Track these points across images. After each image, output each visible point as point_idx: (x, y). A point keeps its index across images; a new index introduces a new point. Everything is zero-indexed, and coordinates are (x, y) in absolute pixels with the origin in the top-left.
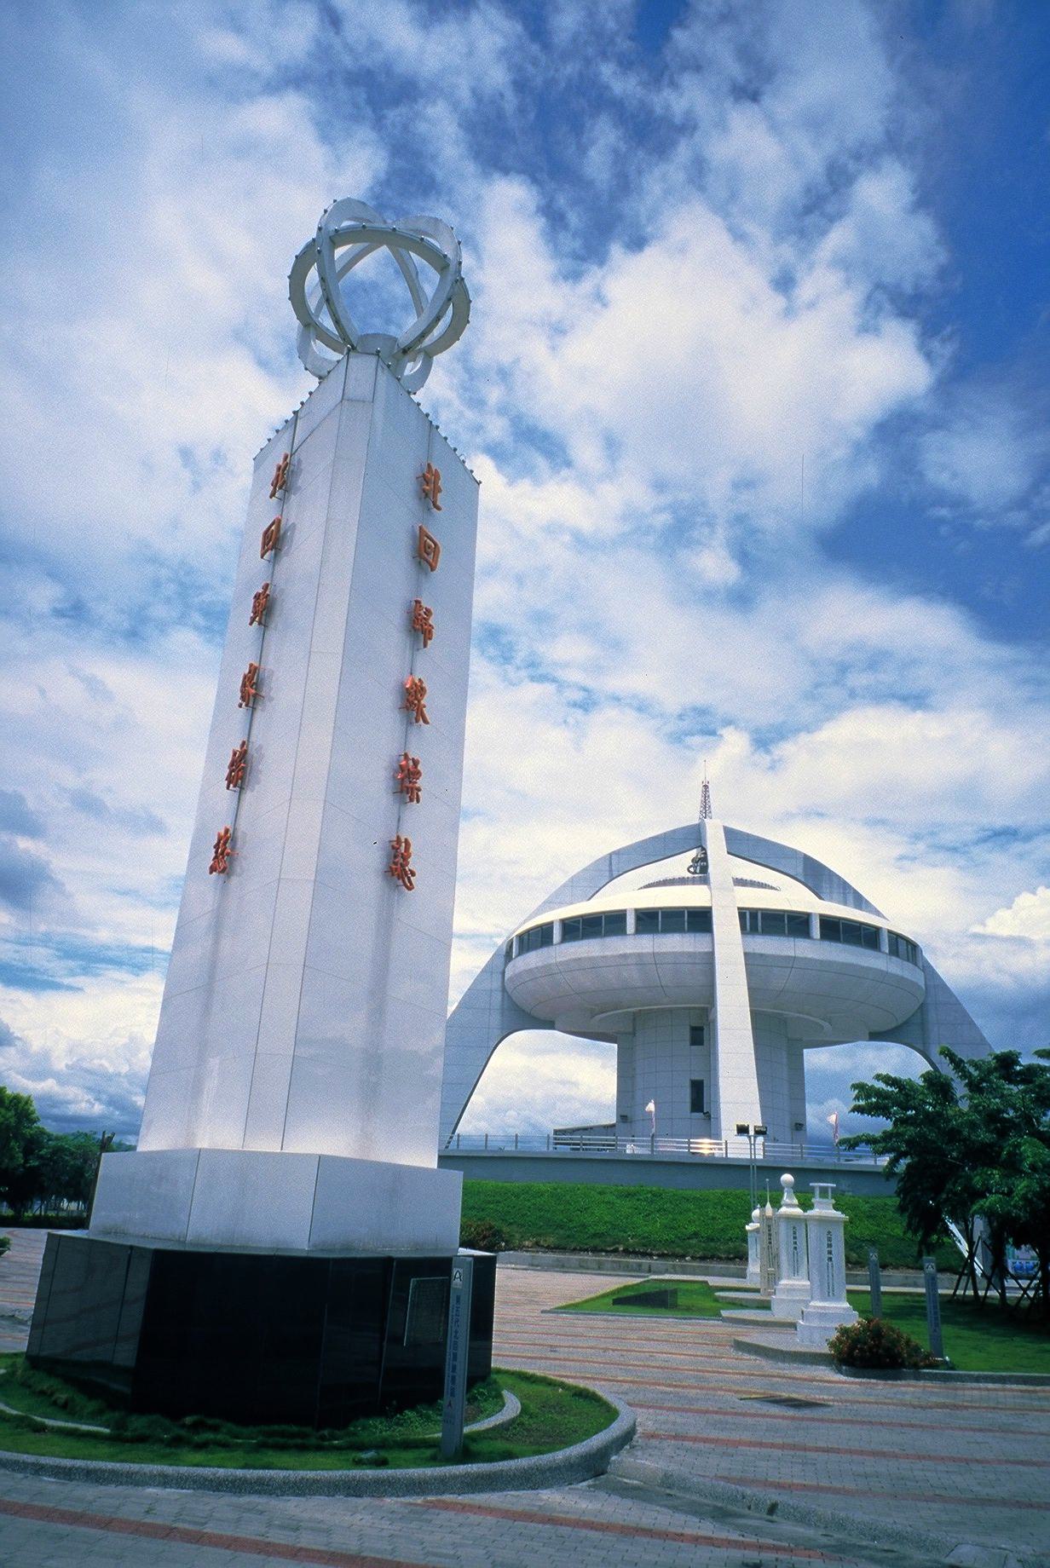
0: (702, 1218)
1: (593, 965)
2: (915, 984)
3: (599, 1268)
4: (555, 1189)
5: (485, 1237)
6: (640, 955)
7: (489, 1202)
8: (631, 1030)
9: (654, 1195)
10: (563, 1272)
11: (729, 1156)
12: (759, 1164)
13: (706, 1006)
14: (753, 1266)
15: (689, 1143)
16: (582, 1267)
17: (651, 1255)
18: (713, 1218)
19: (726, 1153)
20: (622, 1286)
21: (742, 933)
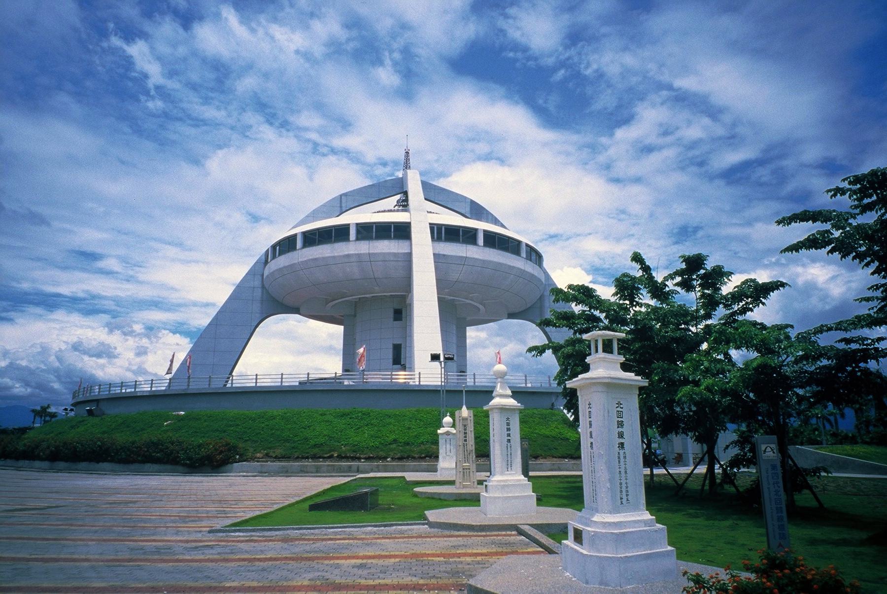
0: (400, 429)
1: (324, 263)
2: (540, 280)
3: (317, 472)
4: (285, 413)
5: (221, 452)
6: (359, 255)
7: (231, 426)
8: (353, 313)
9: (364, 414)
10: (287, 476)
11: (421, 383)
12: (447, 389)
13: (404, 294)
14: (443, 461)
15: (392, 375)
16: (302, 471)
17: (359, 459)
18: (409, 428)
19: (420, 381)
20: (329, 486)
21: (432, 241)
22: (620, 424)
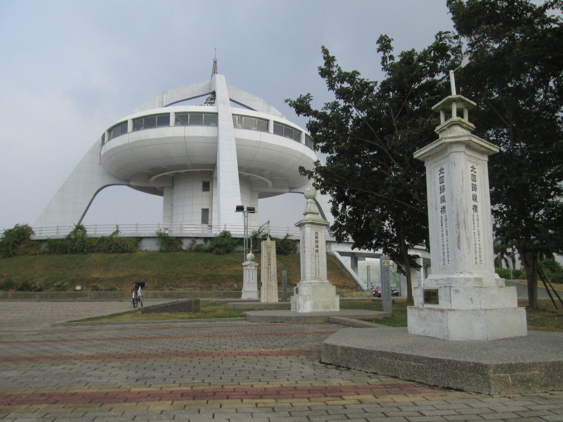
22: (317, 242)
